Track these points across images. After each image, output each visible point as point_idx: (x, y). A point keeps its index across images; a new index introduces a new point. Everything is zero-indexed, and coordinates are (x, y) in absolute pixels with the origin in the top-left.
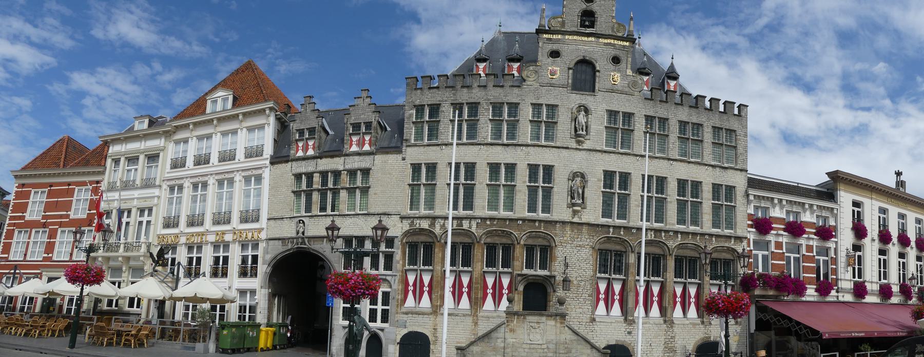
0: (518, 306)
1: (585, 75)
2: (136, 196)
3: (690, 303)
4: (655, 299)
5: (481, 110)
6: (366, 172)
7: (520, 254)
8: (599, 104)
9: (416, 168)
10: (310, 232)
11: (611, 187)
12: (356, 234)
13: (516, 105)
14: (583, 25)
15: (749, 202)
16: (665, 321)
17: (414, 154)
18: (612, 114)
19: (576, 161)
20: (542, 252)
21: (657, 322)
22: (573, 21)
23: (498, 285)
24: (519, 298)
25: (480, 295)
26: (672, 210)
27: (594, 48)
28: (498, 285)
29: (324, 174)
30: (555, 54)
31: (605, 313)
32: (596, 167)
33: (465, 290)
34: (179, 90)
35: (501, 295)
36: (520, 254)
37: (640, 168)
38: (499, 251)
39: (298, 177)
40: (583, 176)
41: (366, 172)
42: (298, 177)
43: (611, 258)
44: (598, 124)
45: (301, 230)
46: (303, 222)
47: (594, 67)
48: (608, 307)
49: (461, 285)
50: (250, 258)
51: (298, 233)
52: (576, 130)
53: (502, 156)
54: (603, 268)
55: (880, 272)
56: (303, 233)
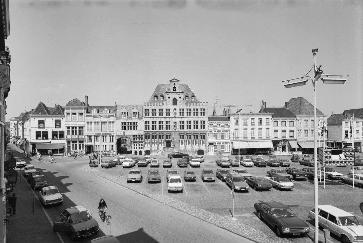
1: (175, 102)
7: (165, 137)
8: (178, 107)
9: (146, 122)
11: (195, 123)
12: (135, 134)
13: (184, 109)
20: (169, 136)
23: (161, 142)
24: (165, 144)
27: (177, 96)
28: (161, 142)
32: (178, 121)
33: (190, 143)
34: (6, 100)
35: (189, 143)
36: (165, 137)
38: (161, 137)
39: (123, 123)
41: (137, 123)
42: (123, 123)
43: (181, 136)
44: (178, 112)
47: (176, 100)
48: (196, 145)
49: (162, 142)
53: (196, 119)
55: (112, 139)
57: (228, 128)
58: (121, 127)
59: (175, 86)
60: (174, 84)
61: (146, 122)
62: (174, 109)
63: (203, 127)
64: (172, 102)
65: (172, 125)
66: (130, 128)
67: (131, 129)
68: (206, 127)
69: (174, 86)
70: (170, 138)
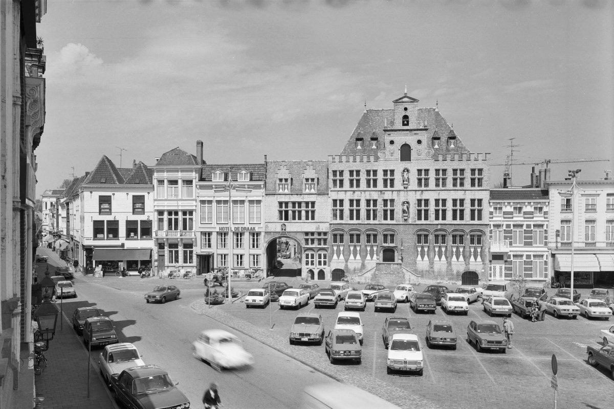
0: (381, 261)
2: (166, 204)
3: (460, 255)
4: (443, 253)
5: (361, 173)
6: (313, 203)
7: (380, 238)
8: (413, 166)
9: (335, 201)
10: (288, 230)
14: (404, 125)
15: (490, 206)
16: (483, 263)
17: (334, 195)
18: (419, 171)
19: (403, 197)
21: (444, 263)
22: (399, 125)
24: (381, 255)
25: (468, 254)
26: (449, 214)
27: (411, 139)
29: (294, 203)
30: (392, 142)
31: (438, 260)
32: (413, 198)
36: (380, 238)
37: (432, 196)
38: (372, 237)
39: (281, 204)
40: (408, 203)
42: (281, 204)
43: (422, 237)
45: (284, 228)
46: (285, 225)
47: (410, 147)
50: (188, 229)
51: (282, 229)
52: (403, 181)
54: (419, 242)
56: (285, 230)
57: (543, 219)
58: (277, 214)
59: (407, 113)
60: (406, 109)
61: (335, 201)
62: (404, 171)
63: (476, 214)
64: (398, 154)
65: (398, 209)
66: (297, 216)
67: (300, 218)
68: (485, 214)
69: (404, 113)
70: (392, 241)
